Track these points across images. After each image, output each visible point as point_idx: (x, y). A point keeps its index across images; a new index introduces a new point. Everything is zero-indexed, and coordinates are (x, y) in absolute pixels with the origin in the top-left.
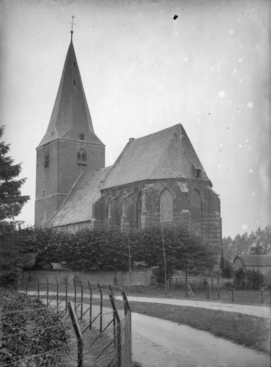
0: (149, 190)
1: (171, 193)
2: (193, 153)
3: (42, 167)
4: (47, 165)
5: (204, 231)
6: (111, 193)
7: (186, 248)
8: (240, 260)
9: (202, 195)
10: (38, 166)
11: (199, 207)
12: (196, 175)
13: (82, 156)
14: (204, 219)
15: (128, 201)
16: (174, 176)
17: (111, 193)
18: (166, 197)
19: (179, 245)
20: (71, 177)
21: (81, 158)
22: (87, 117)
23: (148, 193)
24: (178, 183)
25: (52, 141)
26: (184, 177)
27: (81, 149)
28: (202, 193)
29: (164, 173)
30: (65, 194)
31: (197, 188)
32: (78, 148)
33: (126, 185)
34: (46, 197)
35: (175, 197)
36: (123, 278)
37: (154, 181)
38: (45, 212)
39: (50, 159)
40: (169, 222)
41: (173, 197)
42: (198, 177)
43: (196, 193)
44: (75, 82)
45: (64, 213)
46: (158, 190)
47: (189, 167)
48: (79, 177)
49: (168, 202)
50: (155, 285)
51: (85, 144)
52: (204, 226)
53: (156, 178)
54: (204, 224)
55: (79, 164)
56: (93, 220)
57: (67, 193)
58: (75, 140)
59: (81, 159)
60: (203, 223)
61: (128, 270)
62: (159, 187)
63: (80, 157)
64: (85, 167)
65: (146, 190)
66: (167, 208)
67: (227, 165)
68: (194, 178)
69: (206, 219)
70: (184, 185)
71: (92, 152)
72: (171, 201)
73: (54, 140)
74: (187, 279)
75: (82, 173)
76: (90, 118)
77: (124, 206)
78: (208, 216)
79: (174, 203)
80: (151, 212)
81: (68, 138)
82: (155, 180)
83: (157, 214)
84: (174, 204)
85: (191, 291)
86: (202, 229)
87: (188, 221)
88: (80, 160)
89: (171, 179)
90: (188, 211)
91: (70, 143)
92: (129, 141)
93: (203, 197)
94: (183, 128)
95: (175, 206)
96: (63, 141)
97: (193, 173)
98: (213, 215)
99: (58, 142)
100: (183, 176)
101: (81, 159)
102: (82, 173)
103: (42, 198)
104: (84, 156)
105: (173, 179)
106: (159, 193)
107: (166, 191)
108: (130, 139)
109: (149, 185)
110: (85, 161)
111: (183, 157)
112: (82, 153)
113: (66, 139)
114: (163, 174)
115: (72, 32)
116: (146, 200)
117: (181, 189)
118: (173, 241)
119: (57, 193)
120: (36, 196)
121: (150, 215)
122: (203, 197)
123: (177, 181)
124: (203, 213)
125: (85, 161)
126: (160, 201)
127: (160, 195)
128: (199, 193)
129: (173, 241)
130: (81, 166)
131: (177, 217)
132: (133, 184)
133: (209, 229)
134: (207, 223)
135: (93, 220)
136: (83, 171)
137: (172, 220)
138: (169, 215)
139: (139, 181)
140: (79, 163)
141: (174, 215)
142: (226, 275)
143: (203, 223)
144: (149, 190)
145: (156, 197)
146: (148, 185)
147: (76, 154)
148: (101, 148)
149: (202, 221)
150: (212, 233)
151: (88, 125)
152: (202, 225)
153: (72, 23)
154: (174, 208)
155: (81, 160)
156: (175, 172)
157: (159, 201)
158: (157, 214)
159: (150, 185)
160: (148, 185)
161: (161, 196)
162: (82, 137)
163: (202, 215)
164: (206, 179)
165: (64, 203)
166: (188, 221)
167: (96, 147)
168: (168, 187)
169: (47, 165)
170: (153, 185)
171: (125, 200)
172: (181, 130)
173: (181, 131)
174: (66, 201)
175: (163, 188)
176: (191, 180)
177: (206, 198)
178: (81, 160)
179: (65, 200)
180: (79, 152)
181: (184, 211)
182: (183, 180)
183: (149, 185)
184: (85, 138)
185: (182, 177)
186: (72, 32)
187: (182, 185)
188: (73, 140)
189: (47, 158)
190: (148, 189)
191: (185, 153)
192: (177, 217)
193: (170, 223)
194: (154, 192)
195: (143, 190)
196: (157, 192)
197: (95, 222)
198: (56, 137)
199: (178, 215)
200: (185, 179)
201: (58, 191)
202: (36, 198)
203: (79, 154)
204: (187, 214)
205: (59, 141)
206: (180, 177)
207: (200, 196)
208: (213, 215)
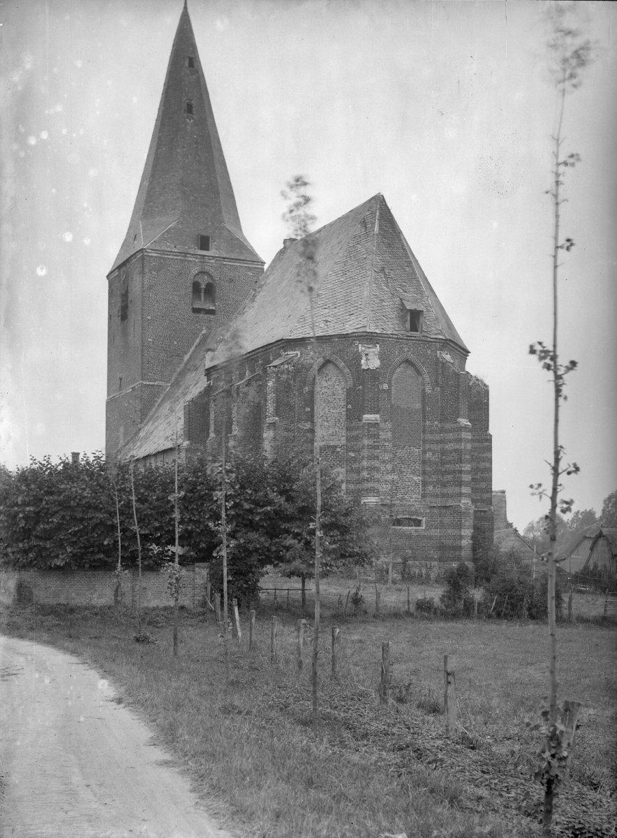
0: (286, 366)
1: (341, 371)
2: (407, 269)
4: (124, 317)
5: (428, 469)
7: (290, 509)
8: (605, 542)
10: (110, 317)
11: (418, 406)
12: (408, 325)
13: (204, 290)
15: (246, 394)
16: (349, 329)
19: (270, 503)
21: (202, 294)
22: (218, 193)
23: (282, 373)
24: (357, 347)
25: (132, 256)
26: (373, 331)
27: (202, 272)
29: (327, 321)
30: (161, 383)
31: (411, 357)
32: (195, 271)
33: (248, 355)
34: (124, 392)
35: (350, 383)
36: (137, 588)
37: (300, 342)
38: (122, 429)
39: (129, 300)
40: (336, 447)
41: (346, 382)
43: (410, 371)
44: (190, 109)
45: (151, 429)
46: (311, 366)
47: (390, 307)
48: (198, 341)
49: (334, 394)
51: (213, 261)
52: (429, 455)
54: (430, 450)
55: (196, 311)
56: (186, 443)
57: (167, 382)
58: (185, 251)
59: (203, 298)
61: (115, 568)
62: (312, 357)
63: (200, 292)
64: (212, 317)
65: (275, 367)
66: (332, 411)
67: (495, 293)
68: (403, 332)
70: (371, 350)
71: (231, 281)
72: (340, 392)
73: (135, 253)
74: (306, 591)
75: (204, 332)
76: (232, 196)
77: (236, 408)
78: (442, 430)
79: (347, 398)
80: (292, 422)
81: (168, 246)
82: (303, 339)
83: (308, 426)
84: (347, 402)
85: (238, 623)
86: (424, 462)
87: (376, 444)
88: (200, 300)
89: (341, 336)
90: (378, 416)
91: (173, 259)
92: (282, 246)
94: (386, 205)
95: (350, 406)
96: (154, 255)
97: (402, 319)
98: (452, 425)
99: (143, 258)
100: (371, 329)
102: (204, 332)
103: (116, 394)
104: (210, 290)
105: (346, 336)
107: (330, 367)
108: (285, 241)
109: (288, 354)
110: (213, 302)
111: (376, 279)
113: (163, 248)
114: (322, 325)
116: (276, 391)
117: (363, 361)
118: (256, 491)
119: (141, 382)
120: (108, 391)
121: (288, 430)
122: (427, 380)
123: (355, 340)
124: (428, 423)
128: (419, 373)
129: (256, 491)
130: (201, 315)
131: (355, 433)
132: (259, 352)
133: (443, 463)
134: (438, 447)
135: (186, 443)
136: (207, 327)
137: (343, 441)
138: (337, 429)
139: (269, 344)
140: (196, 306)
141: (348, 429)
142: (484, 580)
143: (427, 446)
144: (286, 366)
146: (286, 353)
147: (189, 284)
148: (255, 268)
150: (449, 473)
151: (221, 212)
152: (424, 452)
154: (347, 410)
156: (353, 317)
157: (312, 393)
158: (308, 426)
159: (292, 353)
160: (286, 353)
162: (204, 243)
163: (424, 426)
164: (436, 334)
165: (158, 406)
166: (376, 444)
167: (242, 267)
168: (334, 357)
169: (124, 317)
170: (299, 353)
171: (238, 394)
172: (381, 209)
173: (378, 214)
174: (162, 400)
175: (321, 360)
176: (393, 338)
177: (437, 385)
179: (161, 399)
180: (196, 279)
181: (366, 416)
182: (370, 338)
183: (288, 354)
184: (212, 245)
185: (368, 331)
187: (367, 350)
188: (182, 251)
189: (125, 296)
190: (282, 364)
191: (383, 270)
192: (355, 433)
193: (338, 450)
194: (300, 370)
195: (270, 367)
196: (308, 370)
197: (187, 450)
198: (140, 244)
199: (358, 428)
200: (375, 335)
202: (108, 395)
203: (196, 286)
204: (375, 424)
205: (146, 254)
206: (361, 330)
208: (452, 425)
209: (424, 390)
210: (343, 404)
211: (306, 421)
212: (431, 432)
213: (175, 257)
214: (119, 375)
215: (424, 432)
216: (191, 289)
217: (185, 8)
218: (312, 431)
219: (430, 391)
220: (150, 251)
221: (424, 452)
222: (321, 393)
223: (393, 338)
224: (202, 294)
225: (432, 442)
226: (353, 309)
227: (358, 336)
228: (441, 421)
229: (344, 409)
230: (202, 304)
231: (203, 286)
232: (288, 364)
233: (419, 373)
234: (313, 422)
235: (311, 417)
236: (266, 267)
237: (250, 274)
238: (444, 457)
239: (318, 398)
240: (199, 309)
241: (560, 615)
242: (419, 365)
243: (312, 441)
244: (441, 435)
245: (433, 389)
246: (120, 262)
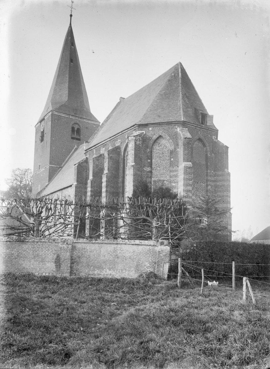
0: (139, 137)
3: (39, 141)
6: (95, 153)
9: (208, 148)
11: (204, 163)
14: (209, 178)
17: (95, 153)
18: (160, 147)
20: (64, 150)
21: (75, 132)
28: (207, 144)
31: (202, 137)
40: (164, 181)
42: (202, 123)
43: (200, 145)
49: (163, 154)
50: (181, 143)
52: (209, 187)
53: (148, 123)
59: (75, 133)
60: (209, 183)
66: (162, 162)
69: (213, 179)
71: (87, 128)
80: (141, 167)
93: (208, 149)
95: (172, 159)
101: (75, 133)
104: (78, 131)
106: (151, 142)
112: (76, 127)
115: (71, 16)
123: (175, 125)
125: (80, 136)
126: (153, 152)
127: (153, 145)
128: (204, 145)
138: (165, 171)
140: (73, 136)
144: (139, 137)
145: (147, 147)
149: (207, 181)
152: (207, 186)
153: (72, 8)
155: (75, 135)
157: (151, 152)
161: (154, 147)
166: (190, 178)
169: (42, 140)
176: (194, 126)
178: (75, 135)
180: (73, 126)
186: (71, 16)
193: (165, 182)
201: (50, 164)
203: (73, 128)
207: (205, 148)
209: (207, 155)
210: (168, 158)
211: (148, 167)
212: (210, 176)
213: (65, 116)
214: (39, 164)
215: (207, 175)
216: (71, 130)
217: (70, 26)
218: (151, 172)
219: (210, 155)
220: (55, 112)
221: (207, 186)
222: (156, 153)
223: (194, 126)
224: (75, 132)
225: (211, 181)
226: (173, 111)
227: (177, 123)
228: (214, 171)
229: (169, 161)
230: (75, 136)
231: (76, 129)
232: (140, 136)
233: (204, 145)
234: (151, 167)
235: (151, 165)
236: (100, 124)
237: (94, 126)
238: (216, 189)
239: (154, 155)
240: (74, 138)
241: (40, 211)
242: (205, 141)
243: (151, 177)
244: (215, 178)
245: (211, 154)
246: (41, 119)
